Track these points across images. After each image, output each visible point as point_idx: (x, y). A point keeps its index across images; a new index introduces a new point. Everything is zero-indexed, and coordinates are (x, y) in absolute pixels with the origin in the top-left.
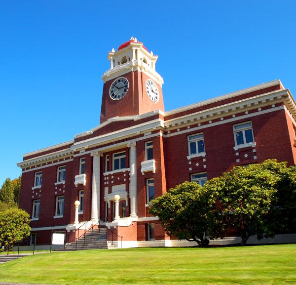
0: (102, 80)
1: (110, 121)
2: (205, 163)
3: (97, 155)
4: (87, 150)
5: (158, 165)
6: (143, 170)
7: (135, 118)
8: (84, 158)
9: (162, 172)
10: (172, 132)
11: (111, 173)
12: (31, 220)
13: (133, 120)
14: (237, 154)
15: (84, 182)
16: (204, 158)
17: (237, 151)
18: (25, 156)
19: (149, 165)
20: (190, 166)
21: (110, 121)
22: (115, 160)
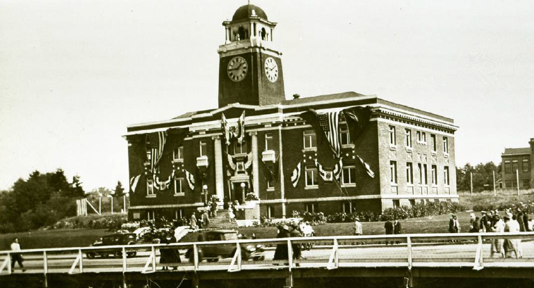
0: (218, 55)
1: (230, 106)
2: (173, 169)
3: (218, 139)
4: (207, 132)
5: (277, 155)
6: (263, 160)
7: (257, 108)
8: (249, 187)
9: (217, 165)
10: (290, 125)
12: (108, 214)
13: (254, 110)
14: (305, 156)
15: (206, 163)
16: (353, 149)
18: (129, 127)
19: (269, 156)
20: (146, 171)
21: (230, 106)
22: (193, 245)
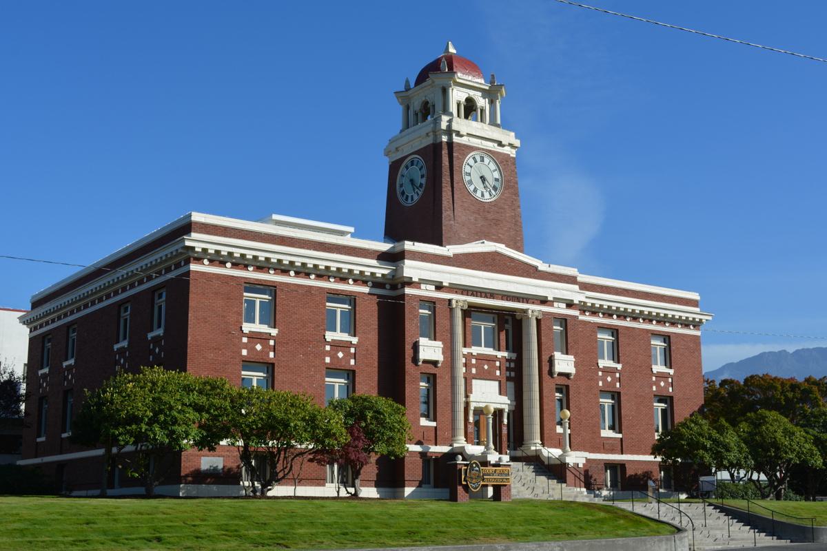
11: (475, 350)
17: (328, 343)
